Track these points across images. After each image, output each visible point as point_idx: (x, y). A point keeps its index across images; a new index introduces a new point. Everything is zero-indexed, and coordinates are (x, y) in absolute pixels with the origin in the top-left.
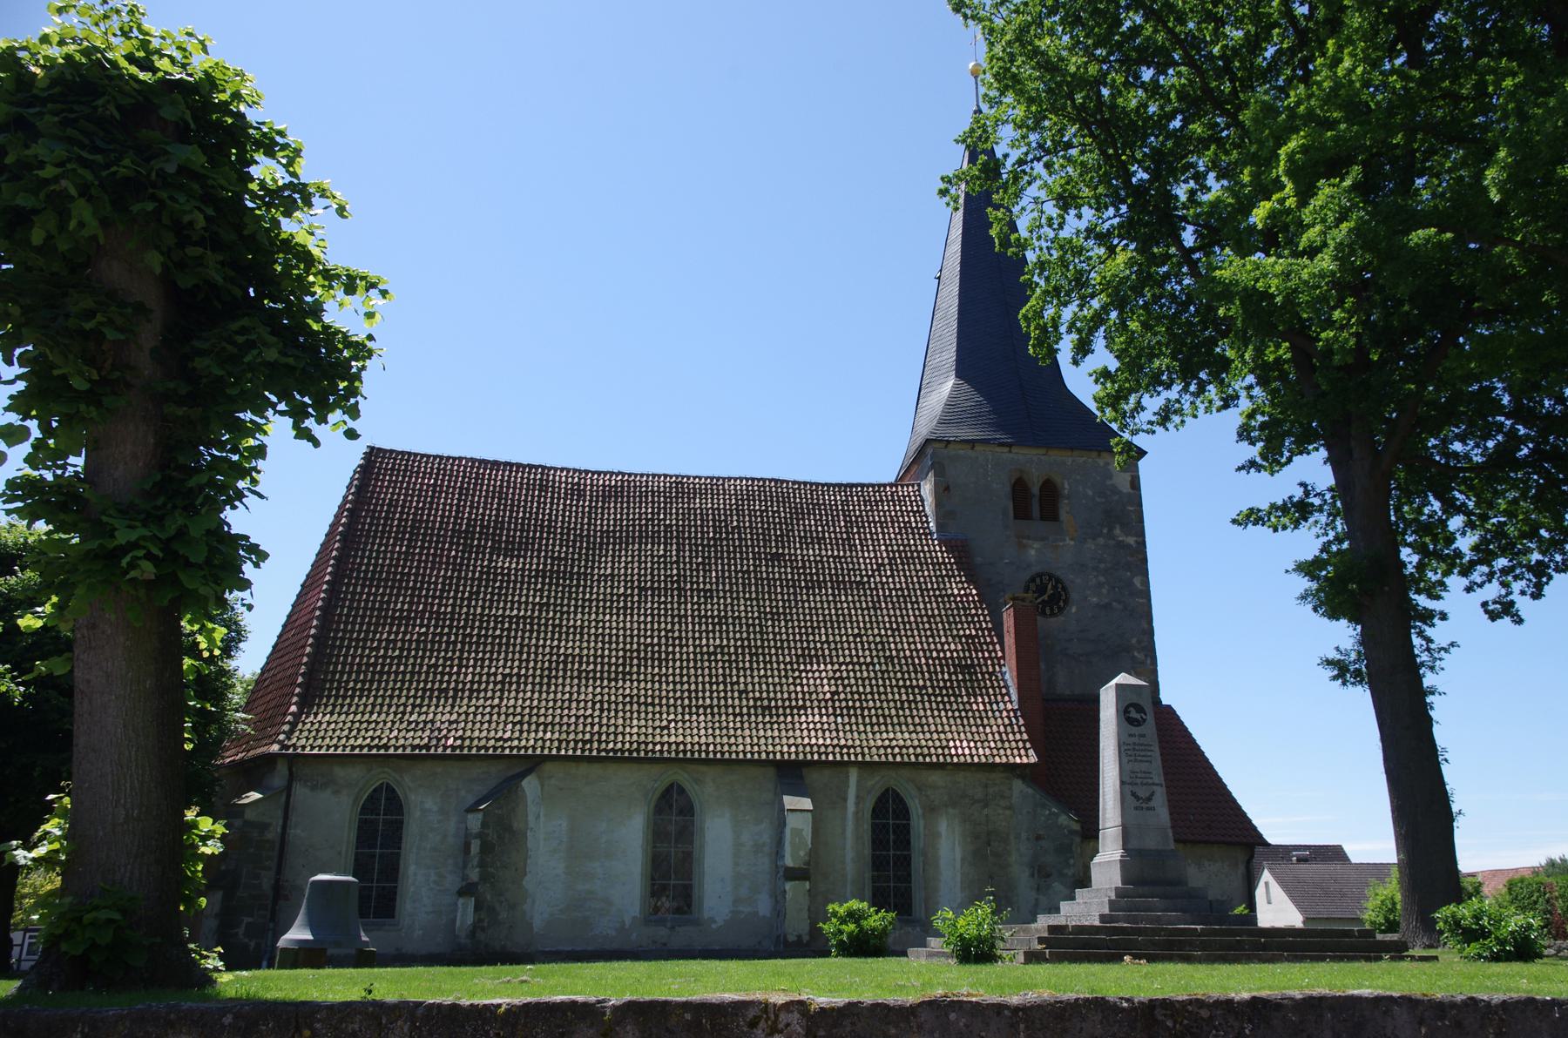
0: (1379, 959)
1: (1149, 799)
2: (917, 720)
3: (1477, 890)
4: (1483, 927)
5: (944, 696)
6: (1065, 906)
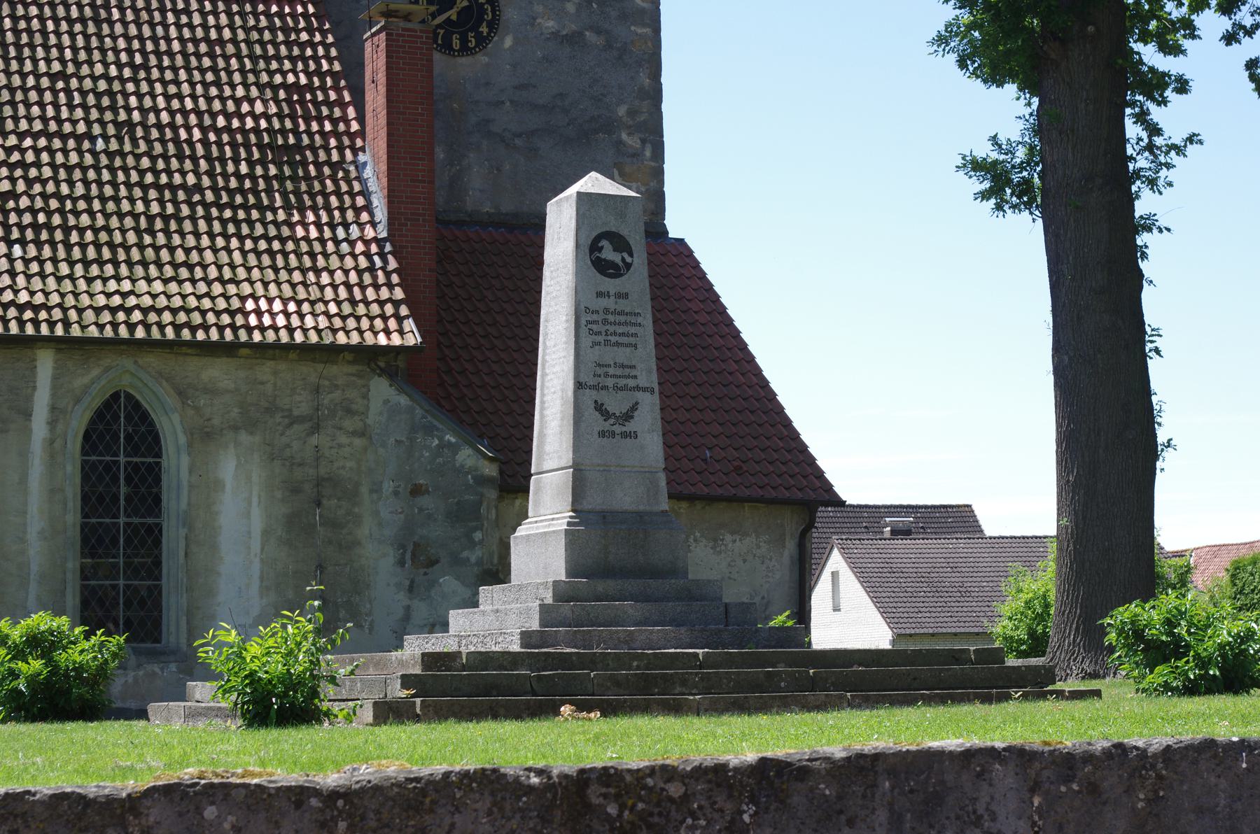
0: (1007, 697)
1: (628, 417)
2: (180, 256)
3: (1183, 581)
4: (1179, 638)
5: (236, 207)
6: (458, 619)
